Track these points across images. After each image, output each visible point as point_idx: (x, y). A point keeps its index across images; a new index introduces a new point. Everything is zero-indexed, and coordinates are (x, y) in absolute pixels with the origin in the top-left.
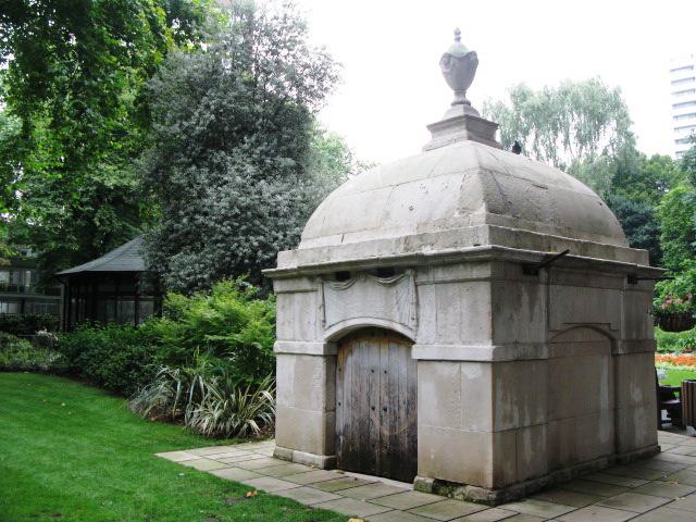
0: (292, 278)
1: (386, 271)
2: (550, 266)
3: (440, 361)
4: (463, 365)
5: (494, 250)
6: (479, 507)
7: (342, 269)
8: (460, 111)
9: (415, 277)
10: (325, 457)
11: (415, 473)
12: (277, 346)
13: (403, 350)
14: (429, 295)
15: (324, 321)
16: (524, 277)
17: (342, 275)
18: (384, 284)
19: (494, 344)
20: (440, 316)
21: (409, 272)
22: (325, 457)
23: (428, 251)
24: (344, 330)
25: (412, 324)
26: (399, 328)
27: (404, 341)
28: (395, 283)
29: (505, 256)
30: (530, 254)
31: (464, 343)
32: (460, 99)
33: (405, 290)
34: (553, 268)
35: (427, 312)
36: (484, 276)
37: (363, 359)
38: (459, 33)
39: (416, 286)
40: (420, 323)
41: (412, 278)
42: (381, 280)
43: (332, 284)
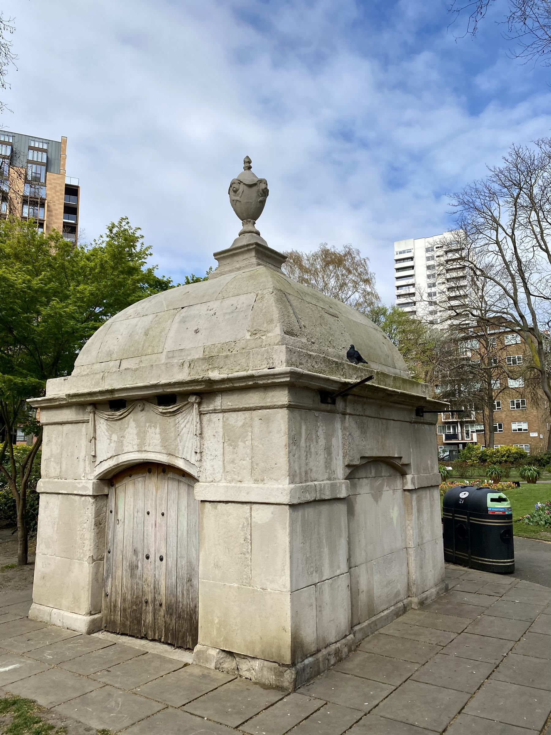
0: (60, 407)
1: (167, 398)
2: (347, 395)
3: (227, 502)
4: (254, 506)
5: (292, 374)
6: (21, 491)
7: (117, 395)
8: (246, 240)
9: (200, 404)
10: (89, 618)
11: (195, 642)
12: (41, 486)
13: (183, 489)
14: (215, 424)
15: (94, 456)
16: (323, 406)
17: (115, 404)
18: (163, 414)
19: (292, 482)
20: (228, 449)
21: (192, 399)
22: (89, 618)
23: (215, 375)
24: (117, 466)
25: (194, 459)
26: (180, 464)
27: (186, 477)
28: (174, 413)
29: (303, 381)
30: (328, 380)
31: (256, 481)
32: (249, 228)
33: (187, 421)
34: (349, 397)
35: (213, 444)
36: (280, 403)
37: (132, 498)
38: (250, 162)
39: (201, 414)
40: (204, 458)
41: (196, 406)
42: (161, 409)
43: (106, 414)
